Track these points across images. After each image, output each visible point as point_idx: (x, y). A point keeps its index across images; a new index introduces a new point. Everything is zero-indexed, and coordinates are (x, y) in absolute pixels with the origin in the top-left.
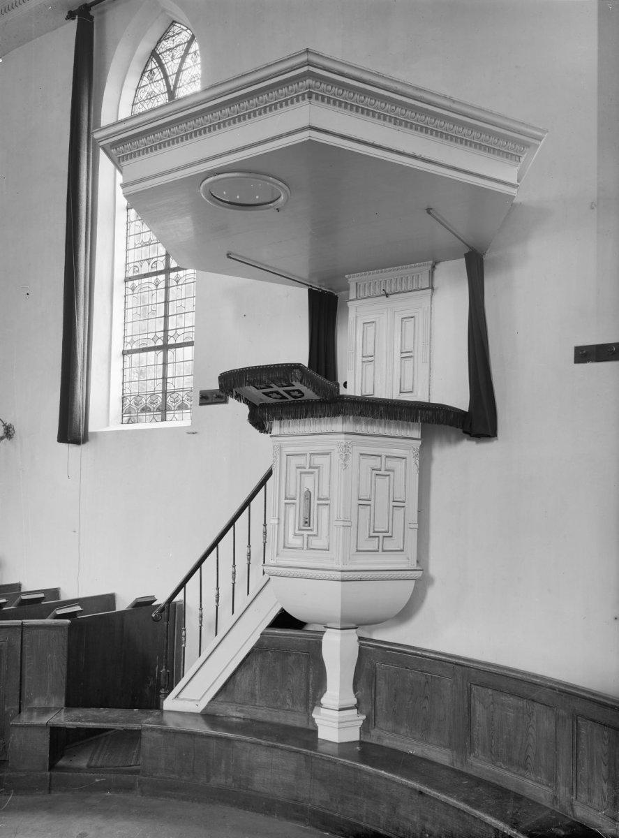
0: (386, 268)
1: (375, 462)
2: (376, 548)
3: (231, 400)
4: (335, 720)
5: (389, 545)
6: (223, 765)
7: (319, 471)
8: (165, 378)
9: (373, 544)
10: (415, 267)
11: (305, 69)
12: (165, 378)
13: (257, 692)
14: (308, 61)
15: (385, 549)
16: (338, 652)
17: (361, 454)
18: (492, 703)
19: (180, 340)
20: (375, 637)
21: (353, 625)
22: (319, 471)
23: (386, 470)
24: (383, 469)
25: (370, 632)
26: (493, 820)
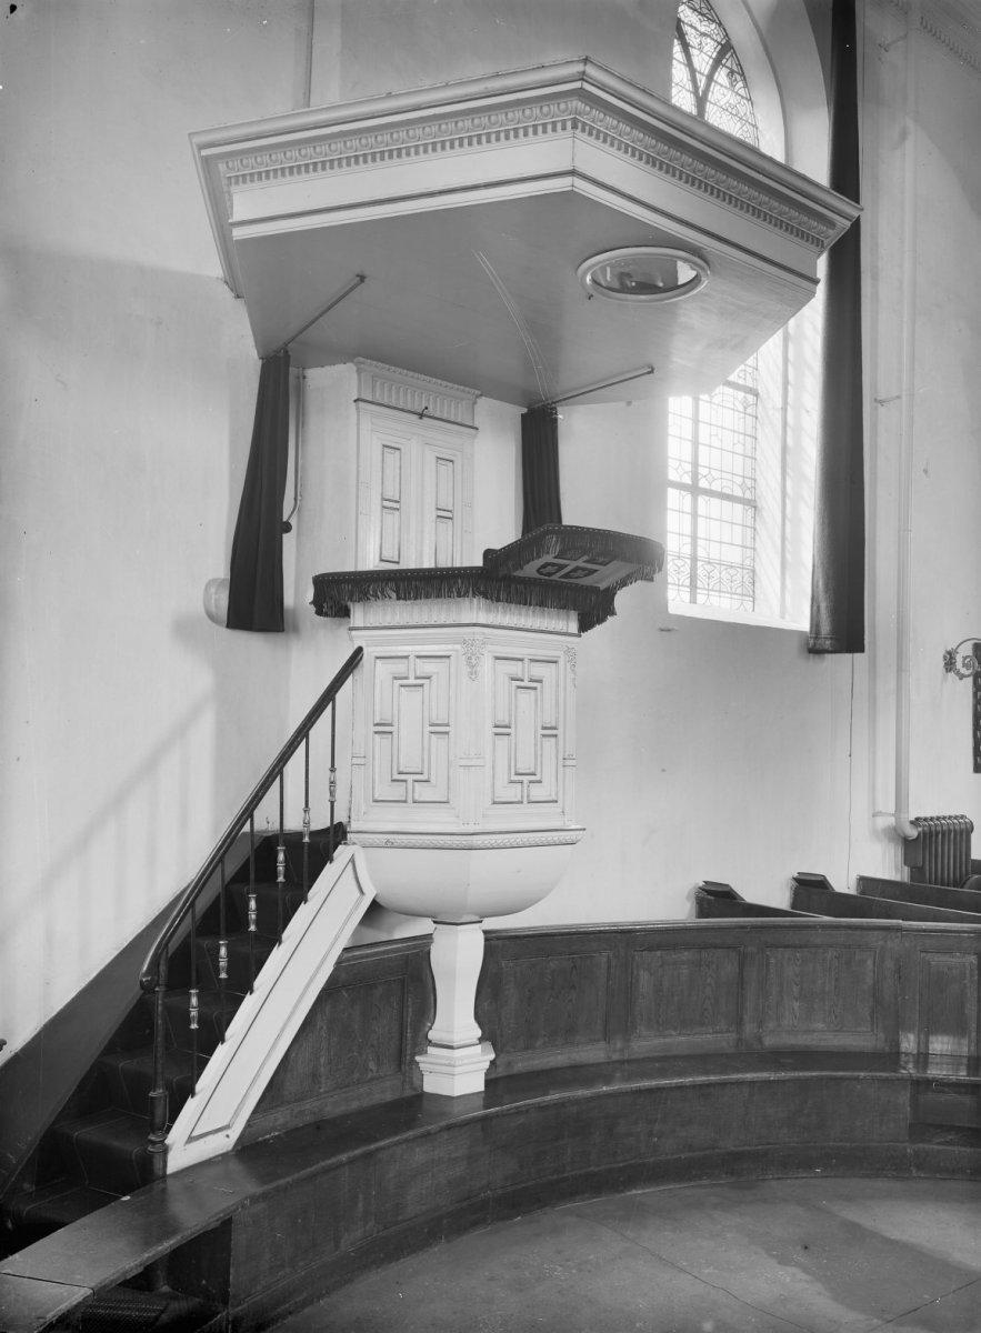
0: (466, 386)
1: (515, 669)
2: (519, 798)
3: (479, 562)
4: (458, 1063)
5: (537, 792)
6: (360, 1205)
7: (542, 687)
8: (694, 538)
9: (397, 792)
10: (463, 391)
11: (577, 85)
12: (694, 538)
13: (322, 1069)
14: (584, 73)
15: (417, 798)
16: (458, 964)
17: (497, 658)
18: (661, 966)
19: (716, 487)
20: (397, 936)
21: (477, 919)
22: (542, 687)
23: (417, 678)
24: (412, 676)
25: (390, 932)
26: (755, 1075)
